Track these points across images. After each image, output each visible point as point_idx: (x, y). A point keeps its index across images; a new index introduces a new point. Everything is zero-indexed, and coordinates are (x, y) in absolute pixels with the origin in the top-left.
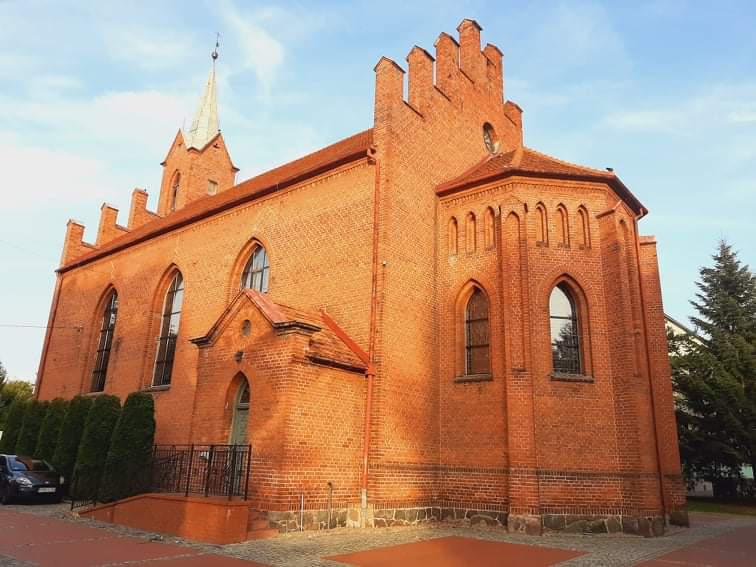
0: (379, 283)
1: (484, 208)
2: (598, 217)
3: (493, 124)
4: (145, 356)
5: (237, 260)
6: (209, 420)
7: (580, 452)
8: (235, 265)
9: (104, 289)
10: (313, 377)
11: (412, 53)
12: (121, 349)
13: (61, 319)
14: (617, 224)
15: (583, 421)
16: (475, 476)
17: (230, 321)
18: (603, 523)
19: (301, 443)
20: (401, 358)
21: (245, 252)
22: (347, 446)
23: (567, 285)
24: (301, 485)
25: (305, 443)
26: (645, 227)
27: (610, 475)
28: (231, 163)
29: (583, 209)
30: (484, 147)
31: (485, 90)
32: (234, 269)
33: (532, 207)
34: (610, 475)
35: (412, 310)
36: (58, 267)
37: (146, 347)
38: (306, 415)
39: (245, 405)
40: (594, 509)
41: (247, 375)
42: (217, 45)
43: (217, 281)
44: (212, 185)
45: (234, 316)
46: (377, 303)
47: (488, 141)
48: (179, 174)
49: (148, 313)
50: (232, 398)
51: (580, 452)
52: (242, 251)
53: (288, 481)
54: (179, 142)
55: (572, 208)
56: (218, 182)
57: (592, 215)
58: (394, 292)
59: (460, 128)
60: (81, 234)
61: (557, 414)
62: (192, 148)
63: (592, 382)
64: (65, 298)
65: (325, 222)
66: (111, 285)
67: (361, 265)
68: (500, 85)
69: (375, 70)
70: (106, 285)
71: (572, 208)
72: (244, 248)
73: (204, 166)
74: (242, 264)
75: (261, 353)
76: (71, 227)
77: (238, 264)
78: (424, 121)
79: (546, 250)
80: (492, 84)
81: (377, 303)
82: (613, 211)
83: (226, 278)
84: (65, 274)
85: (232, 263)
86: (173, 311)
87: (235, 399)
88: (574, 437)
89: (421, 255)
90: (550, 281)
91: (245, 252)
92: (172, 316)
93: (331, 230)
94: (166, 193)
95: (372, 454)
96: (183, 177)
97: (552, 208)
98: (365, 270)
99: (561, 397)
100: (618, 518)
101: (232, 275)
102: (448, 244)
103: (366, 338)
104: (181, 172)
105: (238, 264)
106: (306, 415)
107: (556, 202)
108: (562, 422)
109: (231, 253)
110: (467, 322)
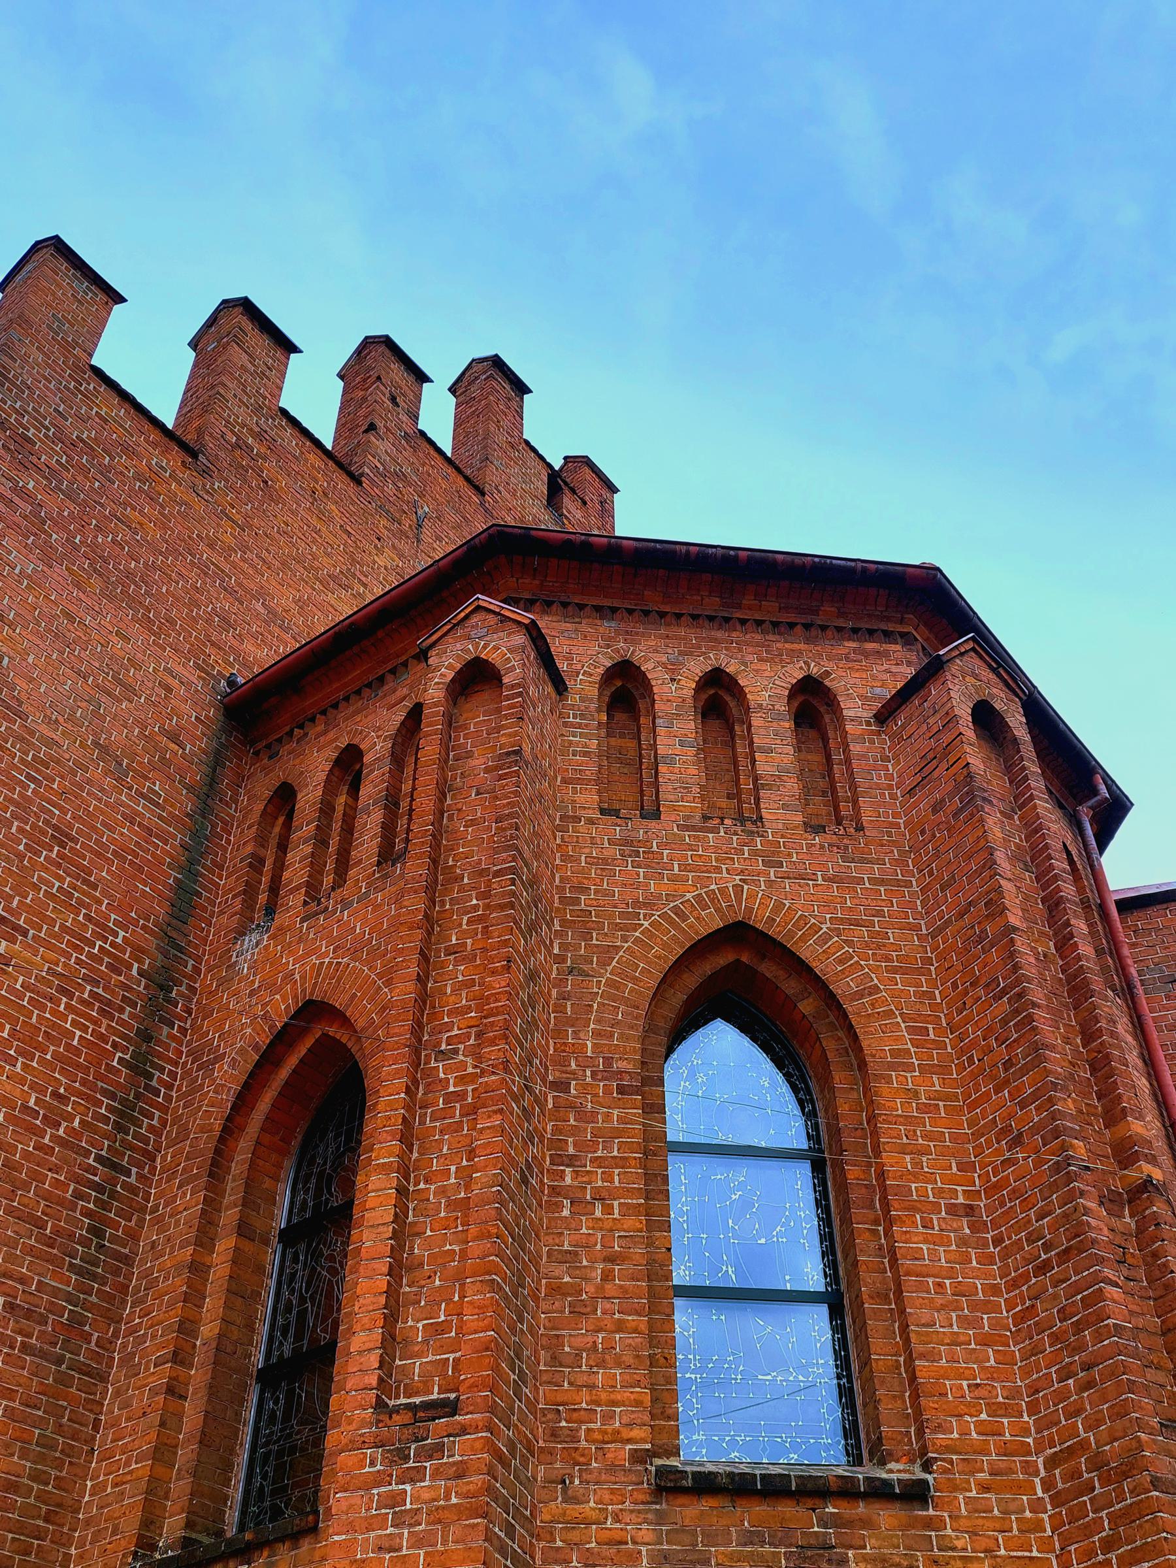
14: (964, 712)
63: (916, 1494)
79: (641, 829)
107: (697, 667)
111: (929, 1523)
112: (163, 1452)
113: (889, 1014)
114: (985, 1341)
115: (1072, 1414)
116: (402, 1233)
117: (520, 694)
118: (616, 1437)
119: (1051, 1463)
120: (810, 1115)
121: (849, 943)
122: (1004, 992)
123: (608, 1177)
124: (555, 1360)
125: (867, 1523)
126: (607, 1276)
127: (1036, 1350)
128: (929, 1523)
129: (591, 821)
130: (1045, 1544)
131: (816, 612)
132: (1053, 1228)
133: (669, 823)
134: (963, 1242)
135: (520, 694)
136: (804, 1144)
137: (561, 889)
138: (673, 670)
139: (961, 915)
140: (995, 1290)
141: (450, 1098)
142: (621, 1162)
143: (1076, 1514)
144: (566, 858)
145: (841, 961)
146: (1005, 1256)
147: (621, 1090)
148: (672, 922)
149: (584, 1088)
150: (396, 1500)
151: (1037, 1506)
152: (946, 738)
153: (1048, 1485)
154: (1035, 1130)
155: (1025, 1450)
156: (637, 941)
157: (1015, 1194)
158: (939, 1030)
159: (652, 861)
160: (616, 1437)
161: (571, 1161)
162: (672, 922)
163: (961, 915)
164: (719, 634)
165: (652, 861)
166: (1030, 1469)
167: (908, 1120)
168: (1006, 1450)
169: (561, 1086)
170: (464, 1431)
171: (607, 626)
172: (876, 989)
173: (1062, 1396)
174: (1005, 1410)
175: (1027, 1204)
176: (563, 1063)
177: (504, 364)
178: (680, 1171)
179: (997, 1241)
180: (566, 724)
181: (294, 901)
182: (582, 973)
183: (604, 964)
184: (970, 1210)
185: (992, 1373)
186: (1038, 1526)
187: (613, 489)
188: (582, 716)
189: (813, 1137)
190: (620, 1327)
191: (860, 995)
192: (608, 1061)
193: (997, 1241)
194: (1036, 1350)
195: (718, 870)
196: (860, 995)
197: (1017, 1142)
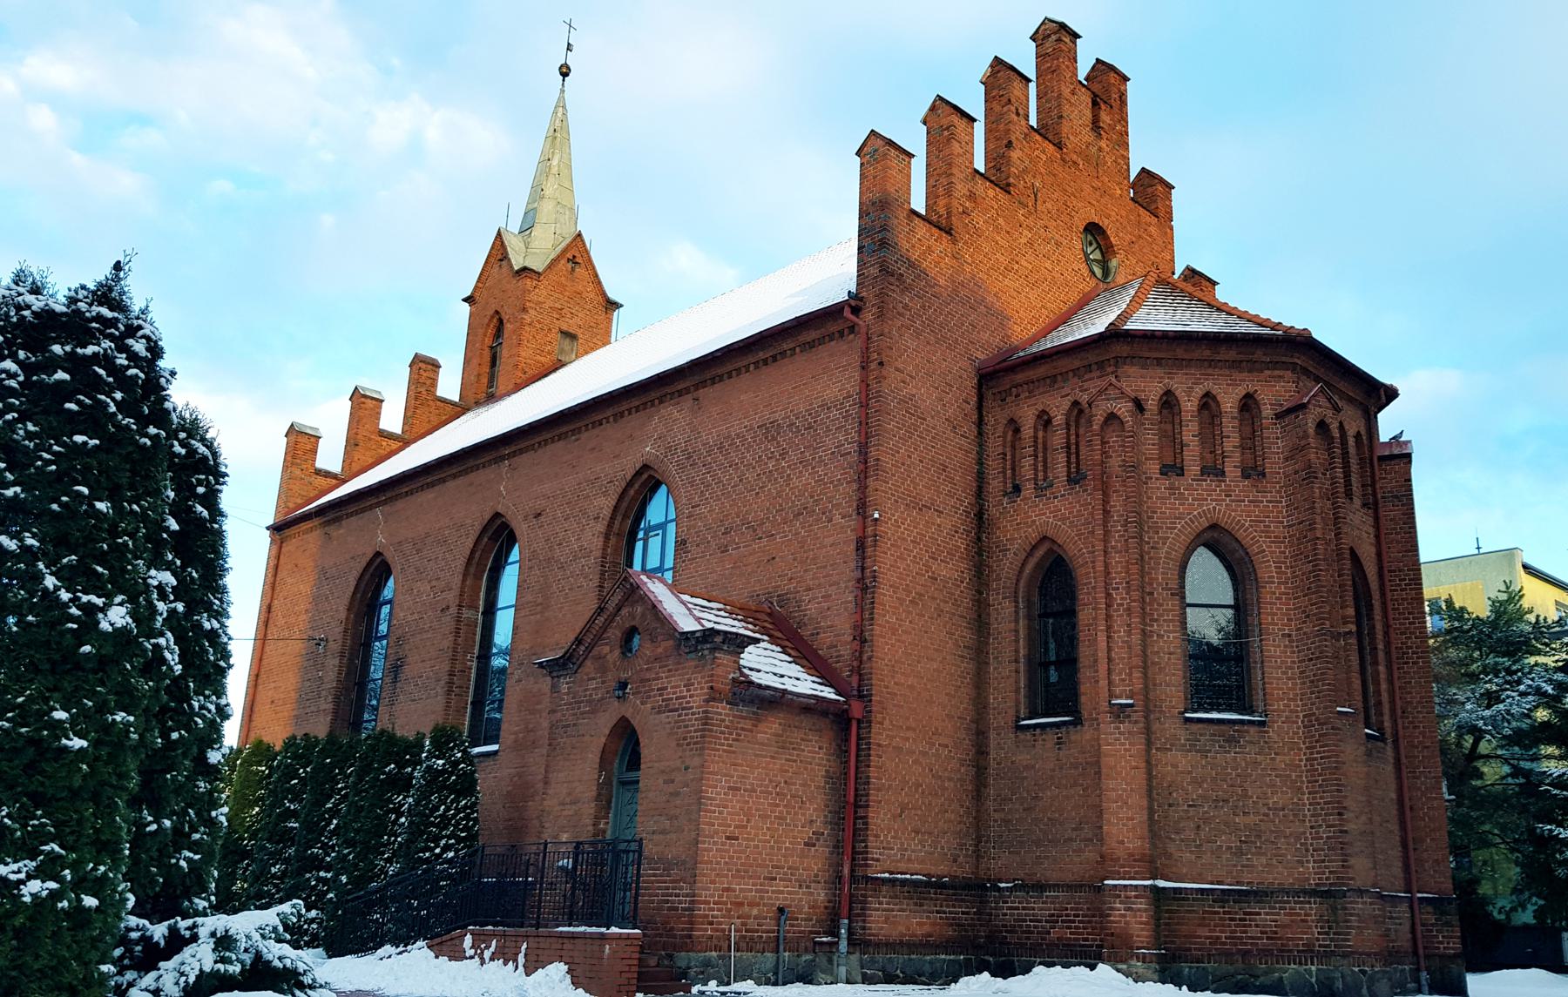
0: (869, 551)
1: (1066, 404)
2: (1279, 416)
3: (1104, 223)
4: (449, 691)
5: (616, 508)
6: (573, 803)
7: (1240, 853)
8: (613, 518)
9: (364, 564)
10: (748, 724)
11: (933, 108)
12: (402, 676)
13: (281, 621)
14: (1311, 429)
15: (1245, 796)
16: (1054, 900)
17: (604, 629)
18: (1281, 979)
19: (728, 838)
20: (911, 687)
21: (632, 492)
22: (814, 845)
23: (1218, 540)
24: (729, 910)
25: (737, 839)
26: (1388, 423)
27: (1297, 893)
28: (604, 294)
29: (1248, 404)
30: (1086, 273)
31: (1087, 159)
32: (610, 525)
33: (1152, 404)
34: (1297, 893)
35: (934, 599)
36: (271, 522)
37: (451, 674)
38: (738, 789)
39: (632, 775)
40: (1265, 953)
41: (635, 723)
42: (565, 72)
43: (581, 548)
44: (567, 341)
45: (611, 619)
46: (865, 586)
47: (1097, 255)
48: (501, 321)
49: (453, 610)
50: (611, 763)
51: (1240, 853)
52: (625, 491)
53: (709, 903)
54: (499, 251)
55: (1229, 402)
56: (579, 333)
57: (1267, 411)
58: (889, 565)
59: (1030, 243)
60: (314, 451)
61: (1197, 783)
62: (525, 269)
63: (1262, 724)
64: (289, 580)
65: (774, 439)
66: (378, 554)
67: (838, 519)
68: (1122, 142)
69: (858, 154)
70: (370, 555)
71: (1229, 402)
72: (630, 484)
73: (549, 303)
74: (625, 516)
75: (656, 685)
76: (293, 438)
77: (619, 518)
78: (954, 242)
79: (1177, 481)
80: (1103, 144)
81: (865, 586)
82: (1303, 407)
83: (598, 543)
84: (287, 532)
85: (607, 513)
86: (513, 609)
87: (616, 765)
88: (1226, 824)
89: (950, 495)
90: (1185, 539)
91: (632, 492)
92: (499, 613)
93: (783, 454)
94: (475, 361)
95: (858, 856)
96: (508, 327)
97: (1189, 405)
98: (843, 529)
99: (1204, 753)
100: (1309, 972)
101: (607, 537)
102: (1004, 472)
103: (846, 651)
104: (505, 318)
105: (619, 518)
106: (738, 789)
107: (1199, 391)
108: (1204, 797)
109: (605, 494)
110: (1039, 616)
111: (1267, 732)
112: (1017, 691)
113: (1269, 561)
114: (1289, 679)
115: (1313, 704)
116: (1109, 649)
117: (1132, 436)
118: (1173, 707)
119: (1304, 716)
120: (1236, 590)
121: (1256, 531)
122: (1310, 562)
123: (1168, 626)
124: (1155, 685)
125: (1248, 732)
126: (1169, 659)
127: (1304, 683)
128: (1267, 732)
129: (1157, 479)
130: (1299, 738)
131: (1253, 354)
132: (1315, 648)
133: (1188, 479)
134: (1285, 646)
135: (1132, 436)
136: (1232, 603)
137: (1147, 512)
138: (1190, 391)
139: (1299, 524)
140: (1294, 662)
141: (1118, 605)
142: (1171, 621)
143: (1309, 732)
144: (1149, 498)
145: (1252, 539)
146: (1299, 652)
147: (1172, 594)
148: (1189, 525)
149: (1159, 594)
150: (1119, 728)
151: (1299, 728)
152: (1303, 443)
153: (1303, 722)
154: (1315, 615)
155: (1297, 711)
156: (1176, 534)
157: (1305, 633)
158: (1287, 568)
159: (1181, 497)
160: (1173, 707)
161: (1156, 620)
162: (1189, 525)
163: (1299, 524)
164: (1210, 371)
165: (1181, 497)
166: (1297, 717)
167: (1271, 603)
168: (1291, 711)
169: (1152, 594)
170: (1136, 712)
171: (1160, 371)
172: (1264, 551)
173: (1310, 698)
174: (1294, 700)
175: (1308, 638)
176: (1151, 584)
177: (1066, 26)
178: (1188, 610)
179: (1297, 647)
180: (1145, 429)
181: (1028, 490)
182: (1157, 549)
183: (1164, 544)
184: (1289, 636)
185: (1290, 689)
186: (1298, 733)
187: (1126, 79)
188: (1152, 424)
189: (1236, 599)
190: (1174, 675)
191: (1258, 553)
192: (1167, 584)
193: (1297, 647)
194: (1304, 683)
195: (1207, 500)
196: (1258, 553)
197: (1307, 616)
